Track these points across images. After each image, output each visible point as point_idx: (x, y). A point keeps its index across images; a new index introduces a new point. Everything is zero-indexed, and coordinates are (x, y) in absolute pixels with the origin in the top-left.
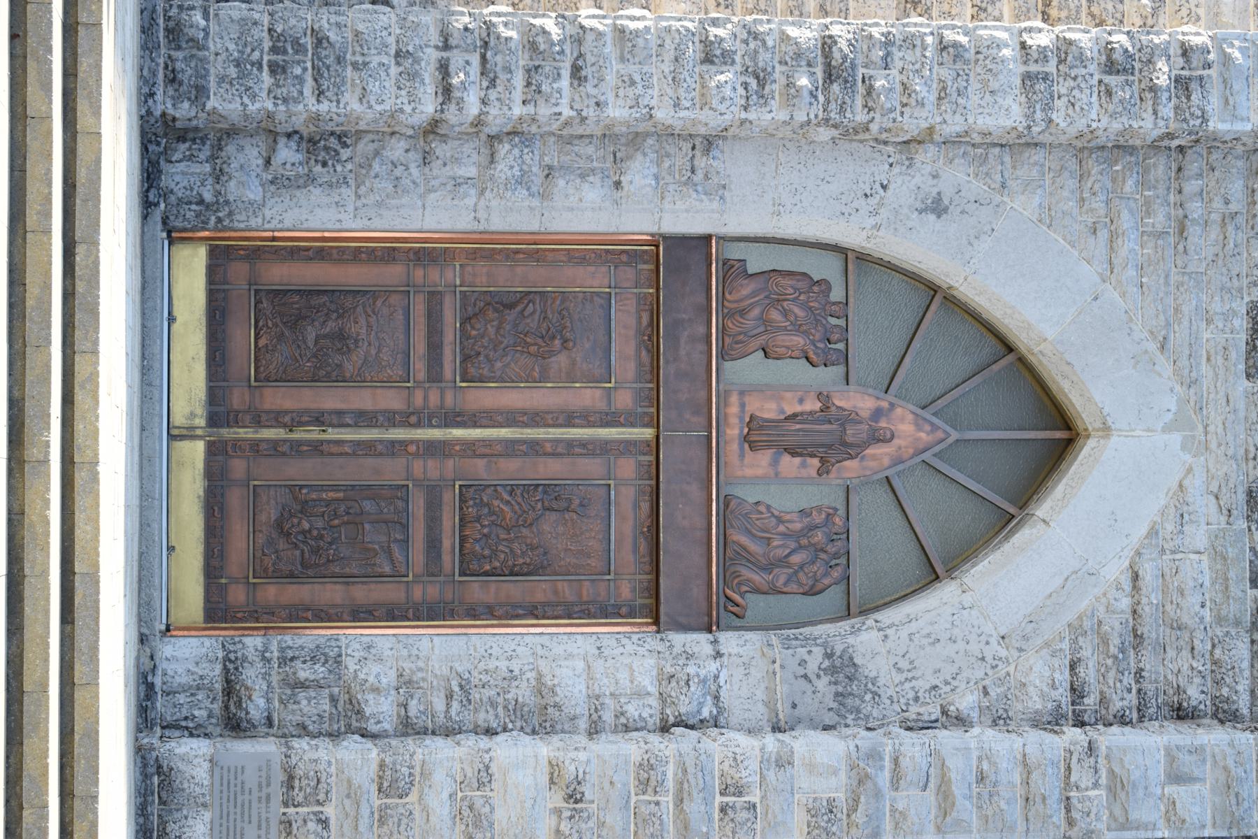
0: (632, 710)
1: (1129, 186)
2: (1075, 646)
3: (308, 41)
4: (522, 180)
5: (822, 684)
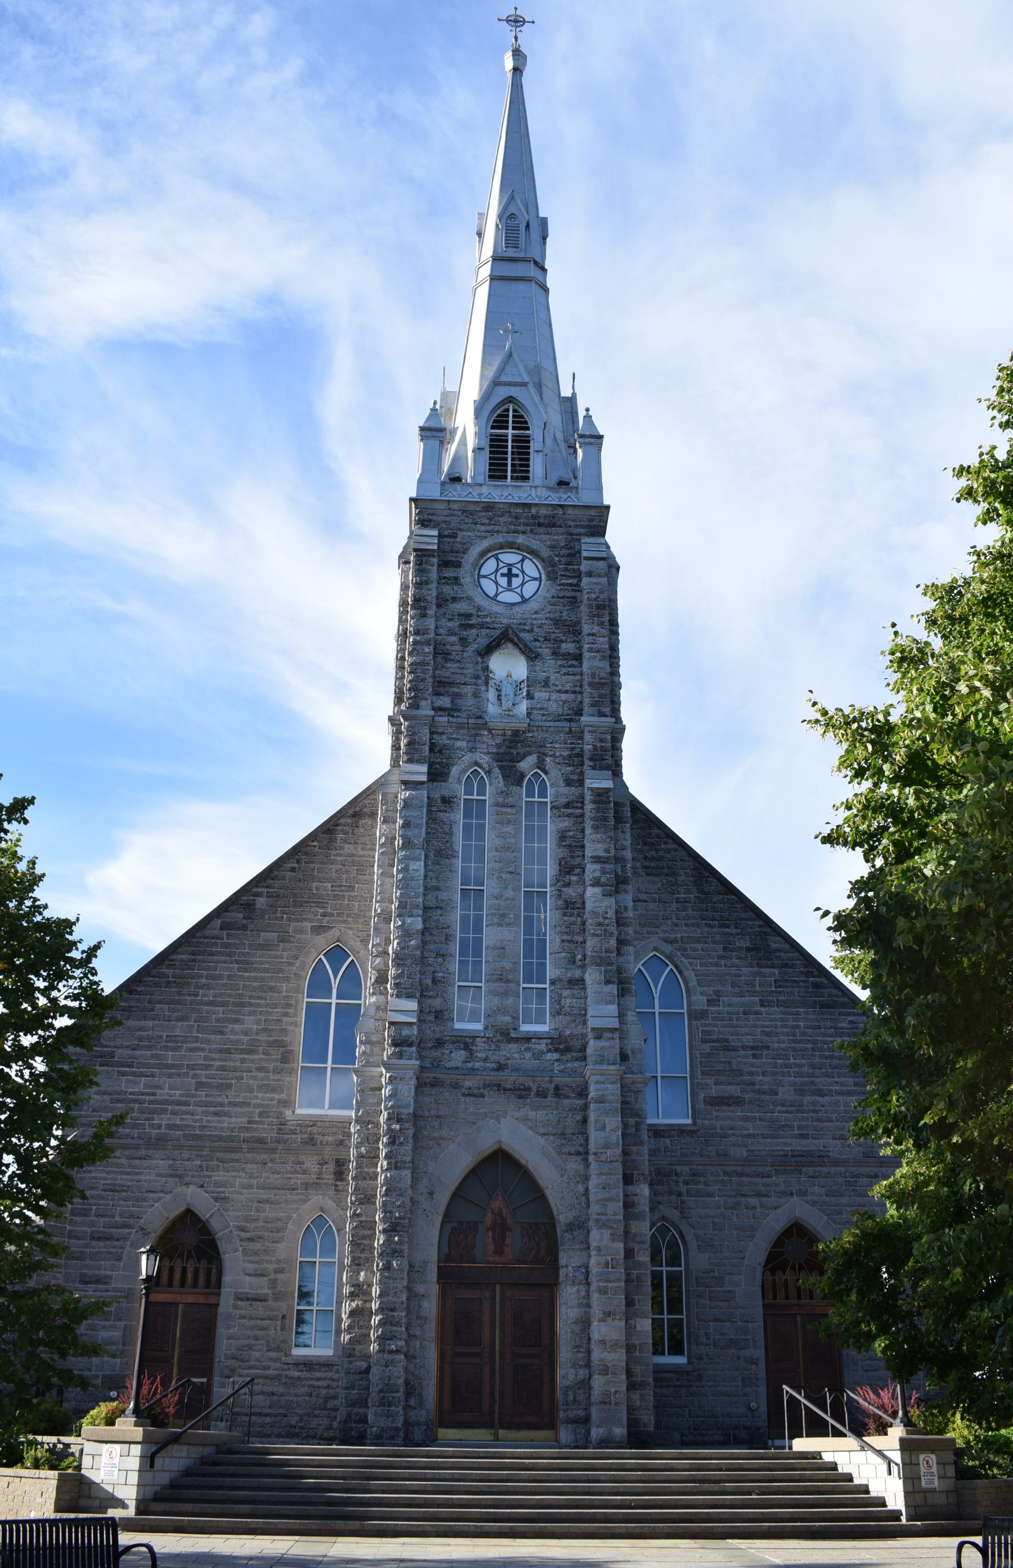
0: (583, 1294)
1: (426, 1133)
2: (565, 1154)
3: (382, 1395)
4: (421, 1326)
5: (575, 1234)
